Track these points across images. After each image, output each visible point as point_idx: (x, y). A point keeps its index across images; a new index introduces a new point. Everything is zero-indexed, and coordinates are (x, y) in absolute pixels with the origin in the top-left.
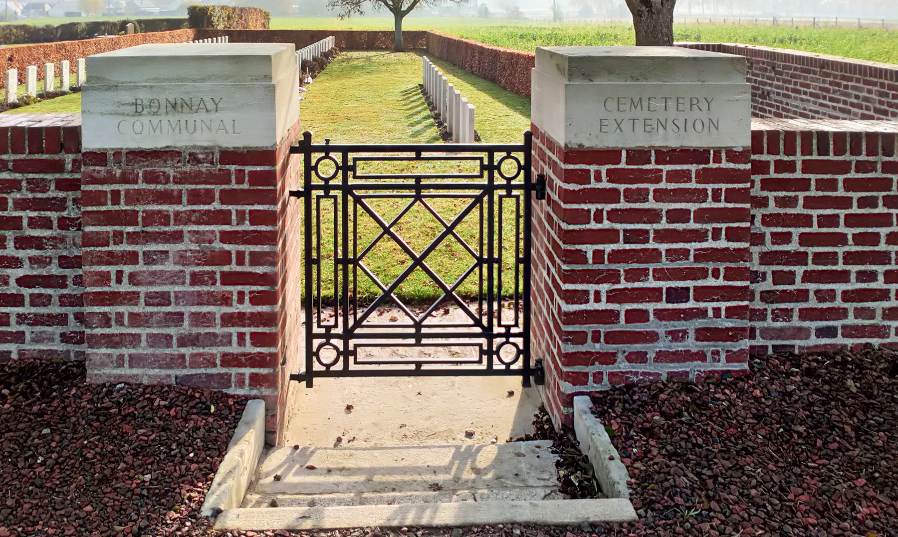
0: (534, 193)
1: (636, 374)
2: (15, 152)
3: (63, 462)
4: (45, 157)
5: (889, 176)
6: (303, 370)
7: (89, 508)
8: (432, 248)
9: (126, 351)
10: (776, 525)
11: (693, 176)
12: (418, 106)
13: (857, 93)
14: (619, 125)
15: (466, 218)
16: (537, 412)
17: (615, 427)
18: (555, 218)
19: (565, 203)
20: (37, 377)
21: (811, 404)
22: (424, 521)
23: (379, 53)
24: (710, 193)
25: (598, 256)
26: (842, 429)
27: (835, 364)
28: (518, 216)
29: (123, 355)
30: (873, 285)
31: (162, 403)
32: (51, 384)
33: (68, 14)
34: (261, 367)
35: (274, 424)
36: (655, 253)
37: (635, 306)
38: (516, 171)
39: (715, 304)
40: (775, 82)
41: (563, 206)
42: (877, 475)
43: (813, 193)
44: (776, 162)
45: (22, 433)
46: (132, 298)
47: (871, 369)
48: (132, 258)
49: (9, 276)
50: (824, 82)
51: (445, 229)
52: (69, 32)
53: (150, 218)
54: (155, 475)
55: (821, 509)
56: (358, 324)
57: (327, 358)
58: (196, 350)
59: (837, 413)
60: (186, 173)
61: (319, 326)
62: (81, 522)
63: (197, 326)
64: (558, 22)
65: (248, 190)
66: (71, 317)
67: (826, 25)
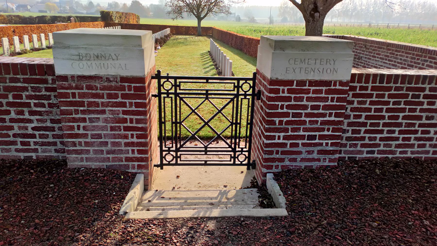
0: (256, 97)
1: (292, 166)
2: (23, 74)
3: (60, 197)
4: (38, 77)
5: (408, 93)
6: (159, 163)
7: (73, 212)
8: (212, 118)
9: (84, 156)
10: (341, 218)
11: (324, 91)
12: (208, 60)
13: (401, 58)
14: (294, 70)
15: (227, 107)
16: (252, 179)
17: (282, 184)
18: (264, 107)
19: (268, 101)
20: (46, 166)
21: (360, 178)
22: (207, 215)
23: (191, 36)
24: (330, 98)
25: (281, 122)
26: (372, 187)
27: (372, 164)
28: (249, 106)
29: (83, 158)
30: (393, 135)
31: (101, 175)
32: (52, 168)
33: (40, 11)
34: (142, 162)
35: (148, 182)
36: (304, 122)
37: (294, 141)
38: (249, 88)
39: (326, 141)
40: (365, 53)
41: (268, 103)
42: (383, 203)
43: (374, 99)
44: (360, 86)
45: (41, 186)
46: (85, 136)
47: (387, 166)
48: (84, 120)
49: (28, 127)
50: (387, 53)
51: (218, 111)
52: (42, 20)
53: (90, 104)
54: (99, 201)
55: (359, 213)
56: (181, 146)
57: (168, 159)
58: (114, 156)
59: (370, 181)
60: (105, 86)
61: (165, 147)
62: (70, 217)
63: (114, 147)
64: (271, 25)
65: (133, 94)
66: (58, 143)
67: (393, 27)
